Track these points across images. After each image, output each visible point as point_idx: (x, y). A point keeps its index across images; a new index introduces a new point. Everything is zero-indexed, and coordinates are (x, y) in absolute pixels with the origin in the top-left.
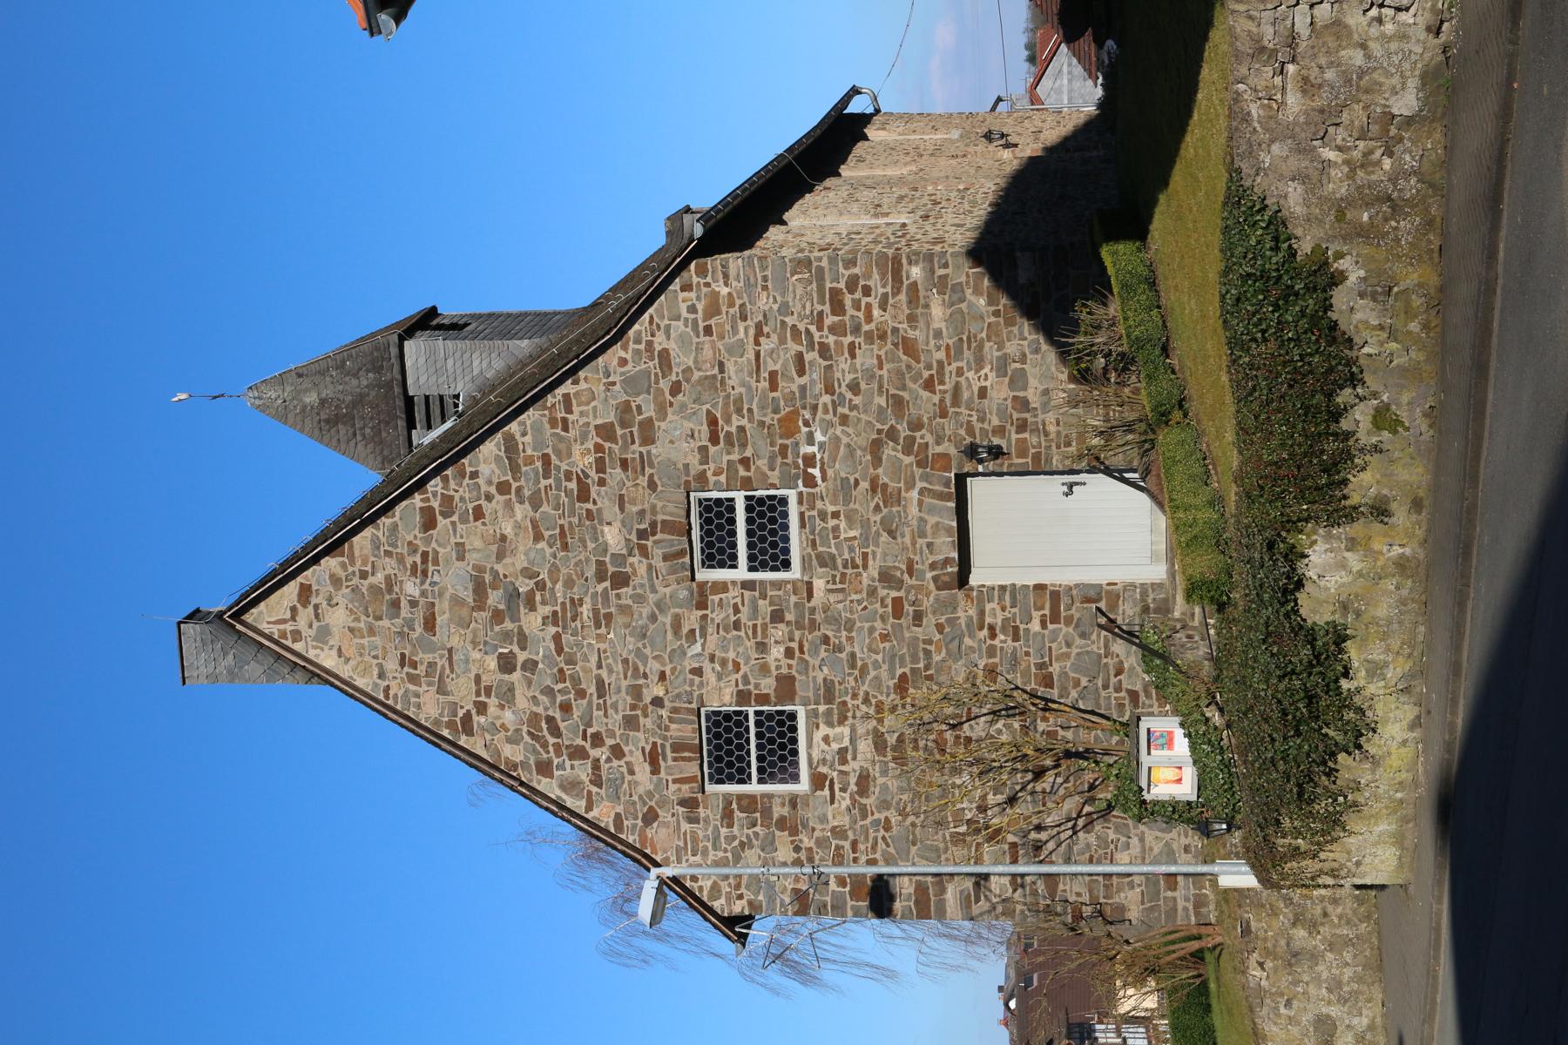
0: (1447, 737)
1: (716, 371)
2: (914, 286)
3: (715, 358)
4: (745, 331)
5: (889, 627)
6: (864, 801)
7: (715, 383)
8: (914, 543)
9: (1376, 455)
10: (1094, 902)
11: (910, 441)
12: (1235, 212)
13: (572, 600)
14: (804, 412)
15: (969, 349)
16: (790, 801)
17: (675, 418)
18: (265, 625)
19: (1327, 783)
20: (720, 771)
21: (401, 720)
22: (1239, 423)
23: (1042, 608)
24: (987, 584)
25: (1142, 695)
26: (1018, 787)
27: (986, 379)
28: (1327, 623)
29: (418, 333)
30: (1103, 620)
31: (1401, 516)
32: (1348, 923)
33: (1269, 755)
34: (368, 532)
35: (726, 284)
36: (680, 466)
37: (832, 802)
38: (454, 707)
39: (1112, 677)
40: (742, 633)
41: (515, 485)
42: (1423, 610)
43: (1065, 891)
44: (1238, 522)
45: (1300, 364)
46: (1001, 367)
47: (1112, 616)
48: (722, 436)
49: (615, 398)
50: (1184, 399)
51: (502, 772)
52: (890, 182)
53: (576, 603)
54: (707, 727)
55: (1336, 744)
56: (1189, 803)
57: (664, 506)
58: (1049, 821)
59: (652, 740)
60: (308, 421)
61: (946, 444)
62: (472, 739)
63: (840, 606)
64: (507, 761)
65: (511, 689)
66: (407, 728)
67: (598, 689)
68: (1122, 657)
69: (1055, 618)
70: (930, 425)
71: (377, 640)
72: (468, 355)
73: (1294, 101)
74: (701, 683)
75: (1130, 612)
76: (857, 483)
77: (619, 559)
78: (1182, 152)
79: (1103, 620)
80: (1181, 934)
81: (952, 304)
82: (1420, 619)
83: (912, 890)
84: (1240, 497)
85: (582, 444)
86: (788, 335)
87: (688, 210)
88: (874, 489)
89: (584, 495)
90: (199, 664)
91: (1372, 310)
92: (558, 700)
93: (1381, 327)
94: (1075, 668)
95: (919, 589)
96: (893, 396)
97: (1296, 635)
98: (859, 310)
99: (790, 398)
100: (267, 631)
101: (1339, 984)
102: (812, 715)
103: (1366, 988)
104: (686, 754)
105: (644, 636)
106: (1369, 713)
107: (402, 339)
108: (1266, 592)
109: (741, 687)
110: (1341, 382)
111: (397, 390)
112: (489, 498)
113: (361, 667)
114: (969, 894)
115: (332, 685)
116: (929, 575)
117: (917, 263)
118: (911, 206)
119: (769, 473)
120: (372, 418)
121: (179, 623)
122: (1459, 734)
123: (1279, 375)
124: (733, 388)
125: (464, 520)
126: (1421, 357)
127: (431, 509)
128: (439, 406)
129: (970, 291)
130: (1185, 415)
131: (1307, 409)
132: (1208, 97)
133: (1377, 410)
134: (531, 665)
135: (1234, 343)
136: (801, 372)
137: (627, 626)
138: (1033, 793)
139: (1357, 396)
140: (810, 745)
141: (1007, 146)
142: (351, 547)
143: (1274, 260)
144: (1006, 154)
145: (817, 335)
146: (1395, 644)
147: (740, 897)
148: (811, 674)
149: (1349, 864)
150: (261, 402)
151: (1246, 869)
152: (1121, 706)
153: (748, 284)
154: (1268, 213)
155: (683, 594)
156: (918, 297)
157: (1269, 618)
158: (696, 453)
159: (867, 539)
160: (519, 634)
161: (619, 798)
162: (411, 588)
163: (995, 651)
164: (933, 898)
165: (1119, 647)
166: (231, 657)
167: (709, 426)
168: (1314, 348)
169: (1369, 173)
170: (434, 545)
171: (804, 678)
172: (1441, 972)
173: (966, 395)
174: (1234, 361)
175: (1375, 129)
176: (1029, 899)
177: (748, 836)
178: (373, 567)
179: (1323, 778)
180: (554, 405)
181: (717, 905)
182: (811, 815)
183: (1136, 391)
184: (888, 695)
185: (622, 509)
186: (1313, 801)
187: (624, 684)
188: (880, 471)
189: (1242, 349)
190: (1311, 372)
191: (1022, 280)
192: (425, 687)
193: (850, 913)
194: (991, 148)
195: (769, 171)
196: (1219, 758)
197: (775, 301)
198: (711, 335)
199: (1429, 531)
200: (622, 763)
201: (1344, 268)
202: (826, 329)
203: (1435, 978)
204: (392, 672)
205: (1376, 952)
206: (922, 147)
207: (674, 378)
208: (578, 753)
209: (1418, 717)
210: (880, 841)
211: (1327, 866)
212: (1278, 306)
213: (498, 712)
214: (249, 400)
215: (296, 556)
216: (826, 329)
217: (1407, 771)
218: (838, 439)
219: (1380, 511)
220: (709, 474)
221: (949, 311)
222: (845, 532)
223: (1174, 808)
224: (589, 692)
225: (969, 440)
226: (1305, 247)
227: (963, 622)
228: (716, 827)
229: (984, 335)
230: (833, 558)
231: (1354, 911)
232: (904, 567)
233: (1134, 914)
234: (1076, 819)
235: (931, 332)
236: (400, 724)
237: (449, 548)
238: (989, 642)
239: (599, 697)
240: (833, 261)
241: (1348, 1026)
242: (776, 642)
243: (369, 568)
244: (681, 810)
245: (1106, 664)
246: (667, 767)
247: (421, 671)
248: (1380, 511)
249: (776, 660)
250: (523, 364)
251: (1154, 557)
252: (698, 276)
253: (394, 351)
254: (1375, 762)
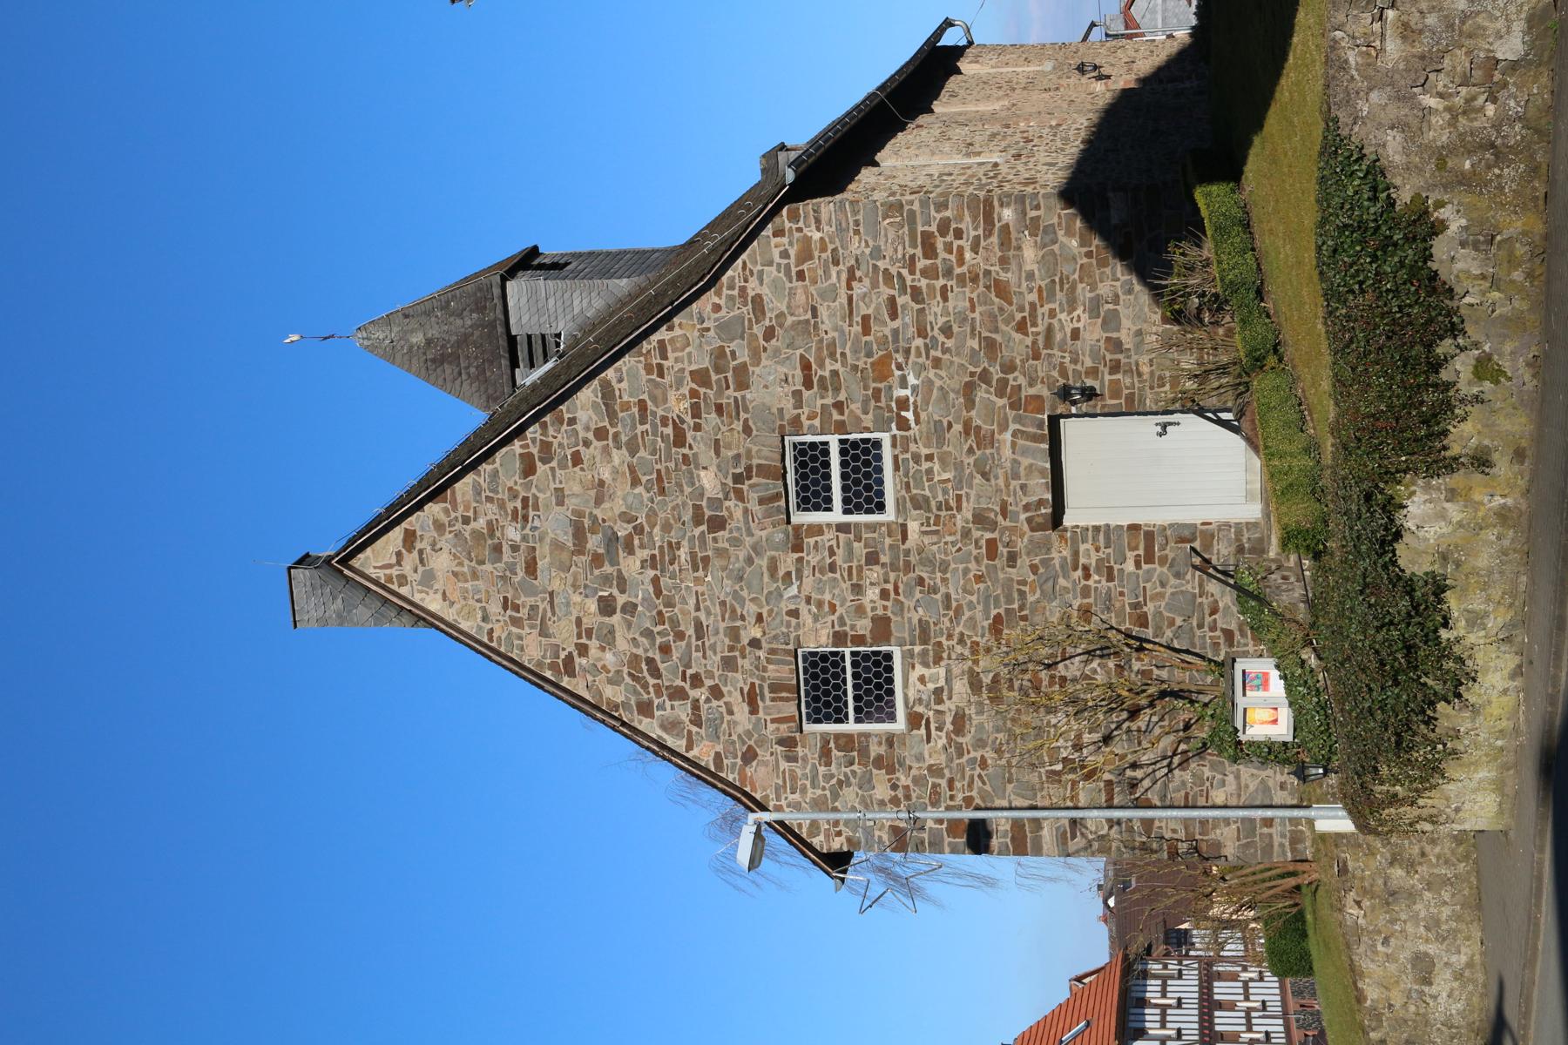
0: (1550, 690)
1: (809, 315)
2: (1006, 229)
3: (807, 303)
4: (837, 276)
5: (983, 568)
6: (960, 740)
7: (808, 327)
8: (1007, 485)
9: (1477, 406)
10: (1190, 839)
11: (1003, 383)
12: (1332, 162)
13: (670, 544)
14: (897, 356)
15: (1062, 290)
16: (887, 740)
17: (769, 363)
18: (372, 570)
19: (1425, 731)
20: (817, 711)
21: (505, 663)
22: (1336, 375)
23: (1136, 548)
24: (1081, 524)
25: (1237, 634)
26: (1113, 726)
27: (1079, 320)
28: (1426, 574)
29: (520, 274)
30: (1197, 561)
31: (1503, 467)
32: (1446, 862)
33: (1367, 705)
34: (469, 478)
35: (818, 229)
36: (775, 410)
37: (929, 741)
38: (556, 649)
39: (1207, 616)
40: (838, 575)
41: (612, 431)
42: (1524, 561)
43: (1160, 828)
44: (1335, 473)
45: (1398, 315)
46: (1094, 308)
47: (1206, 556)
48: (815, 380)
49: (711, 344)
50: (1279, 344)
51: (603, 712)
52: (983, 119)
53: (674, 547)
54: (804, 668)
55: (1435, 694)
56: (1285, 744)
57: (759, 451)
58: (1144, 759)
59: (750, 680)
60: (414, 361)
61: (1039, 386)
62: (574, 681)
63: (935, 548)
64: (609, 701)
65: (612, 632)
66: (510, 670)
67: (696, 631)
68: (1217, 597)
69: (1149, 559)
70: (1023, 367)
71: (480, 584)
72: (569, 293)
73: (1393, 47)
74: (798, 624)
75: (1224, 552)
76: (950, 425)
77: (715, 503)
78: (1277, 95)
79: (1197, 561)
80: (1278, 871)
81: (1044, 246)
82: (1522, 569)
83: (1008, 827)
84: (1337, 449)
85: (678, 389)
86: (881, 279)
87: (782, 147)
88: (967, 431)
89: (680, 440)
90: (310, 608)
91: (1474, 259)
92: (658, 643)
93: (1483, 277)
94: (1169, 607)
95: (1013, 530)
96: (986, 338)
97: (1394, 586)
98: (951, 252)
99: (883, 342)
100: (373, 576)
101: (1437, 923)
102: (908, 656)
103: (1464, 927)
104: (784, 694)
105: (741, 579)
106: (1469, 663)
107: (504, 280)
108: (1363, 544)
109: (837, 628)
110: (1441, 332)
111: (500, 329)
112: (587, 444)
113: (466, 610)
114: (1065, 832)
115: (437, 628)
116: (1023, 517)
117: (1008, 205)
118: (1003, 144)
119: (863, 417)
120: (476, 358)
121: (289, 568)
122: (1562, 688)
123: (1376, 326)
124: (826, 333)
125: (563, 466)
126: (1525, 306)
127: (530, 455)
128: (541, 346)
129: (1062, 232)
130: (1280, 360)
131: (1406, 360)
132: (1301, 40)
133: (1478, 360)
134: (630, 608)
135: (1330, 295)
136: (894, 315)
137: (724, 569)
138: (1129, 731)
139: (1458, 346)
140: (906, 685)
141: (1100, 78)
142: (453, 493)
143: (1372, 210)
144: (1099, 87)
145: (909, 279)
146: (1496, 593)
147: (839, 834)
148: (906, 615)
149: (1448, 810)
150: (370, 343)
151: (1343, 813)
152: (1216, 645)
153: (841, 230)
154: (1366, 162)
155: (779, 537)
156: (1010, 239)
157: (1366, 569)
158: (790, 398)
159: (961, 481)
160: (618, 577)
161: (718, 738)
162: (513, 533)
163: (1089, 591)
164: (1029, 835)
165: (1213, 587)
166: (339, 601)
167: (802, 370)
168: (1413, 299)
169: (1471, 120)
170: (534, 490)
171: (899, 619)
172: (1543, 920)
173: (1058, 337)
174: (1331, 313)
175: (1478, 74)
176: (1126, 836)
177: (846, 775)
178: (475, 512)
179: (1422, 726)
180: (649, 352)
181: (816, 842)
182: (908, 754)
183: (1230, 333)
184: (983, 636)
185: (717, 453)
186: (1412, 748)
187: (722, 626)
188: (973, 413)
189: (1339, 301)
190: (1410, 323)
191: (1115, 220)
192: (527, 630)
193: (947, 849)
194: (1084, 80)
195: (866, 106)
196: (1315, 699)
197: (867, 245)
198: (804, 280)
199: (1531, 481)
200: (721, 703)
201: (1445, 217)
202: (918, 272)
203: (1537, 925)
204: (495, 614)
205: (1475, 891)
206: (1015, 80)
207: (767, 323)
208: (679, 694)
209: (1520, 666)
210: (976, 778)
211: (1425, 813)
212: (1376, 256)
213: (600, 654)
214: (358, 340)
215: (400, 502)
216: (918, 272)
217: (1508, 719)
218: (930, 383)
219: (1482, 462)
220: (803, 418)
221: (1041, 253)
222: (939, 474)
223: (1270, 749)
224: (688, 634)
225: (1062, 381)
226: (1404, 196)
227: (1057, 562)
228: (814, 765)
229: (1076, 276)
230: (927, 499)
231: (1453, 853)
232: (998, 509)
233: (1230, 850)
234: (1172, 757)
235: (1024, 275)
236: (504, 666)
237: (548, 494)
238: (1083, 582)
239: (698, 639)
240: (924, 204)
241: (1446, 964)
242: (872, 584)
243: (471, 514)
244: (780, 749)
245: (1201, 604)
246: (765, 708)
247: (523, 613)
248: (1482, 462)
249: (872, 601)
250: (623, 303)
251: (1249, 496)
252: (790, 222)
253: (497, 291)
254: (1475, 710)
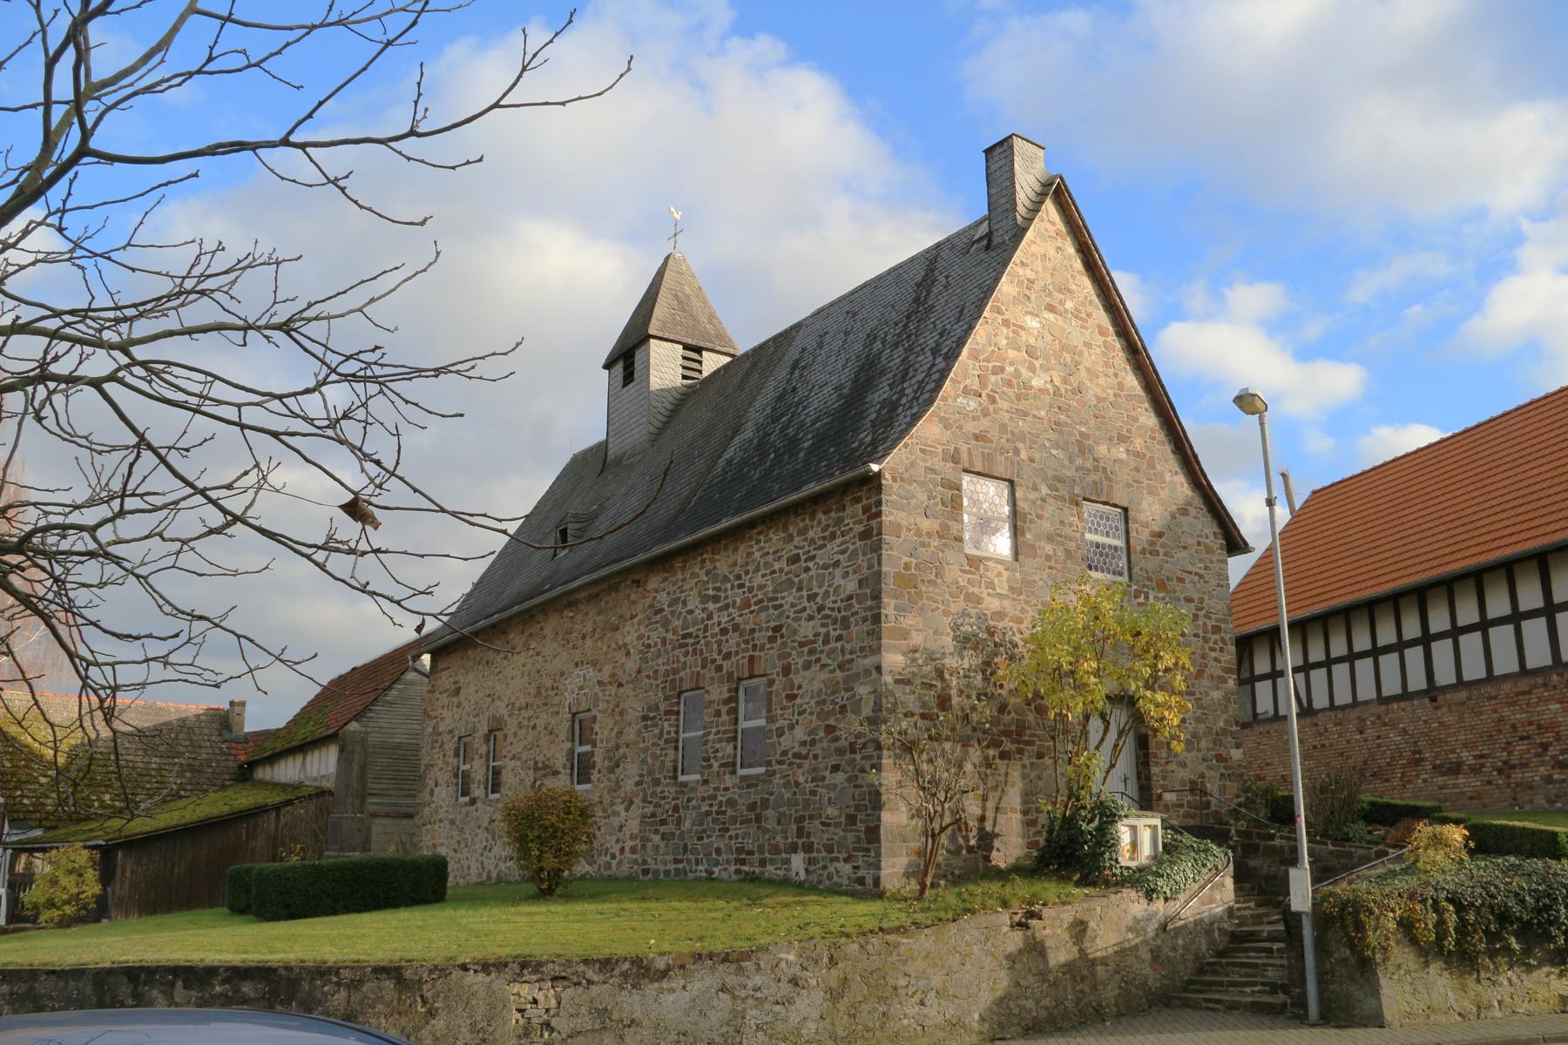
111: (710, 345)
162: (1069, 305)
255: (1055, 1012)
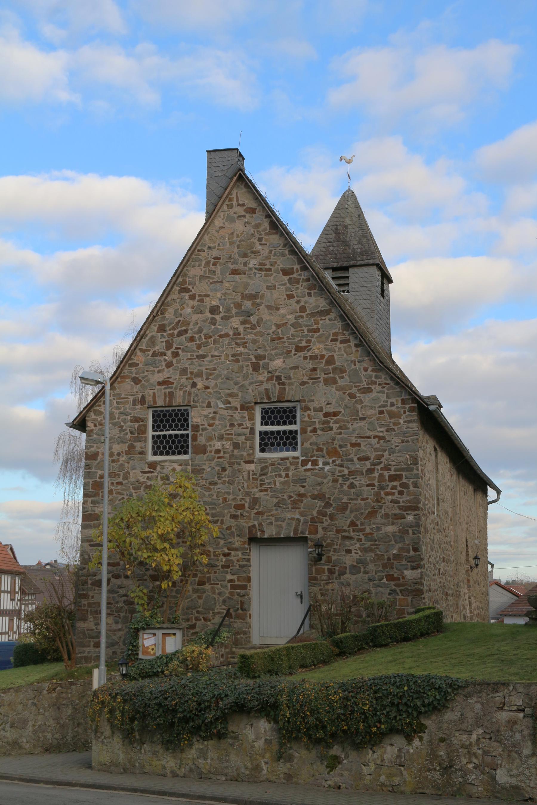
111: (352, 263)
255: (61, 742)
